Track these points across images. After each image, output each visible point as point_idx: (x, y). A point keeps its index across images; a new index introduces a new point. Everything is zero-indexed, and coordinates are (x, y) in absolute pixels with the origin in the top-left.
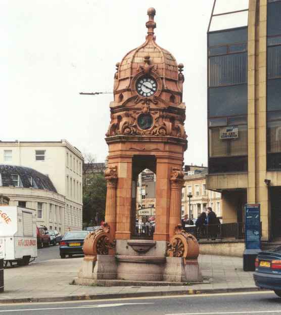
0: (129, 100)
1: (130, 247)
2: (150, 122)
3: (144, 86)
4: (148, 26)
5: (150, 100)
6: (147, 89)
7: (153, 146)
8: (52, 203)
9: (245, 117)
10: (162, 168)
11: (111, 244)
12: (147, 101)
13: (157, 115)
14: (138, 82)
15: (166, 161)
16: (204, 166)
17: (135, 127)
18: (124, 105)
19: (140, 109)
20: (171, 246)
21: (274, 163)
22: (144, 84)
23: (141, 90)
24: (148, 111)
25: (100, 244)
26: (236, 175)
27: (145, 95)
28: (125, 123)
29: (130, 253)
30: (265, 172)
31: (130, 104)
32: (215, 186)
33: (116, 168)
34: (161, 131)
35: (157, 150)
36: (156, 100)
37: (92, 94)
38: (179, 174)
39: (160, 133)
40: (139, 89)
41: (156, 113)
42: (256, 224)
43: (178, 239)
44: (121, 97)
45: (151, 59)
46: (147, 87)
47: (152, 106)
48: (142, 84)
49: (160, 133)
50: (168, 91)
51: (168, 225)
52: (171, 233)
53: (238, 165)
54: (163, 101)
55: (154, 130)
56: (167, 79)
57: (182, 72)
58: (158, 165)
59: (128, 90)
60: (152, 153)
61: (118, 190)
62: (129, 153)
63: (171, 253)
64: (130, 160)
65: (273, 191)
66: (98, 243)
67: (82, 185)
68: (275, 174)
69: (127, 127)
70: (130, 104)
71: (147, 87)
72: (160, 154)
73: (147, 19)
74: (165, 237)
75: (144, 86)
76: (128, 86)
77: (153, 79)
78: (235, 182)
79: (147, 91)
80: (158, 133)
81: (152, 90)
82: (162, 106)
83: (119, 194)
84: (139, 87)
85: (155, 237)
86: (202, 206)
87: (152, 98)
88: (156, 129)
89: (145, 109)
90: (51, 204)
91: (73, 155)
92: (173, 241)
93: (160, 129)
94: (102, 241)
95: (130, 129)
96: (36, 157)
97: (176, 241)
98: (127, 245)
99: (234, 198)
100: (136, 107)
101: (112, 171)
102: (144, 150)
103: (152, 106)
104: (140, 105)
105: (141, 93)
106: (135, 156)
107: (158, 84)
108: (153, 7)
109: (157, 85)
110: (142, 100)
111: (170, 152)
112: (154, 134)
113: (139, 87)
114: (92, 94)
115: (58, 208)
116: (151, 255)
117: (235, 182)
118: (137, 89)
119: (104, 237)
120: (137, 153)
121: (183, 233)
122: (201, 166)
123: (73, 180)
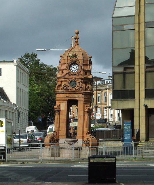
0: (66, 74)
2: (76, 84)
3: (73, 67)
5: (76, 74)
6: (74, 69)
7: (77, 95)
8: (7, 110)
10: (81, 105)
13: (78, 81)
14: (70, 66)
18: (64, 76)
19: (71, 78)
20: (84, 142)
21: (150, 94)
23: (72, 69)
26: (126, 101)
27: (73, 71)
28: (64, 85)
29: (67, 145)
30: (144, 99)
31: (67, 76)
32: (116, 106)
33: (60, 105)
34: (80, 89)
36: (78, 74)
38: (88, 109)
41: (79, 80)
43: (87, 138)
46: (74, 68)
47: (77, 77)
48: (72, 67)
51: (83, 132)
52: (85, 135)
53: (130, 95)
55: (77, 88)
57: (91, 60)
59: (65, 69)
60: (76, 99)
61: (61, 116)
62: (66, 98)
63: (84, 145)
65: (150, 112)
66: (51, 140)
67: (28, 94)
70: (67, 76)
71: (74, 68)
74: (82, 137)
75: (73, 67)
76: (66, 67)
78: (128, 105)
80: (79, 90)
82: (81, 77)
83: (61, 118)
85: (77, 137)
87: (76, 74)
89: (73, 79)
90: (6, 111)
91: (22, 71)
92: (85, 139)
93: (80, 88)
97: (87, 139)
99: (128, 114)
100: (69, 77)
101: (58, 106)
102: (73, 97)
103: (77, 77)
104: (71, 76)
105: (72, 70)
109: (79, 67)
110: (72, 74)
115: (11, 113)
117: (128, 105)
118: (70, 69)
119: (54, 137)
123: (19, 89)
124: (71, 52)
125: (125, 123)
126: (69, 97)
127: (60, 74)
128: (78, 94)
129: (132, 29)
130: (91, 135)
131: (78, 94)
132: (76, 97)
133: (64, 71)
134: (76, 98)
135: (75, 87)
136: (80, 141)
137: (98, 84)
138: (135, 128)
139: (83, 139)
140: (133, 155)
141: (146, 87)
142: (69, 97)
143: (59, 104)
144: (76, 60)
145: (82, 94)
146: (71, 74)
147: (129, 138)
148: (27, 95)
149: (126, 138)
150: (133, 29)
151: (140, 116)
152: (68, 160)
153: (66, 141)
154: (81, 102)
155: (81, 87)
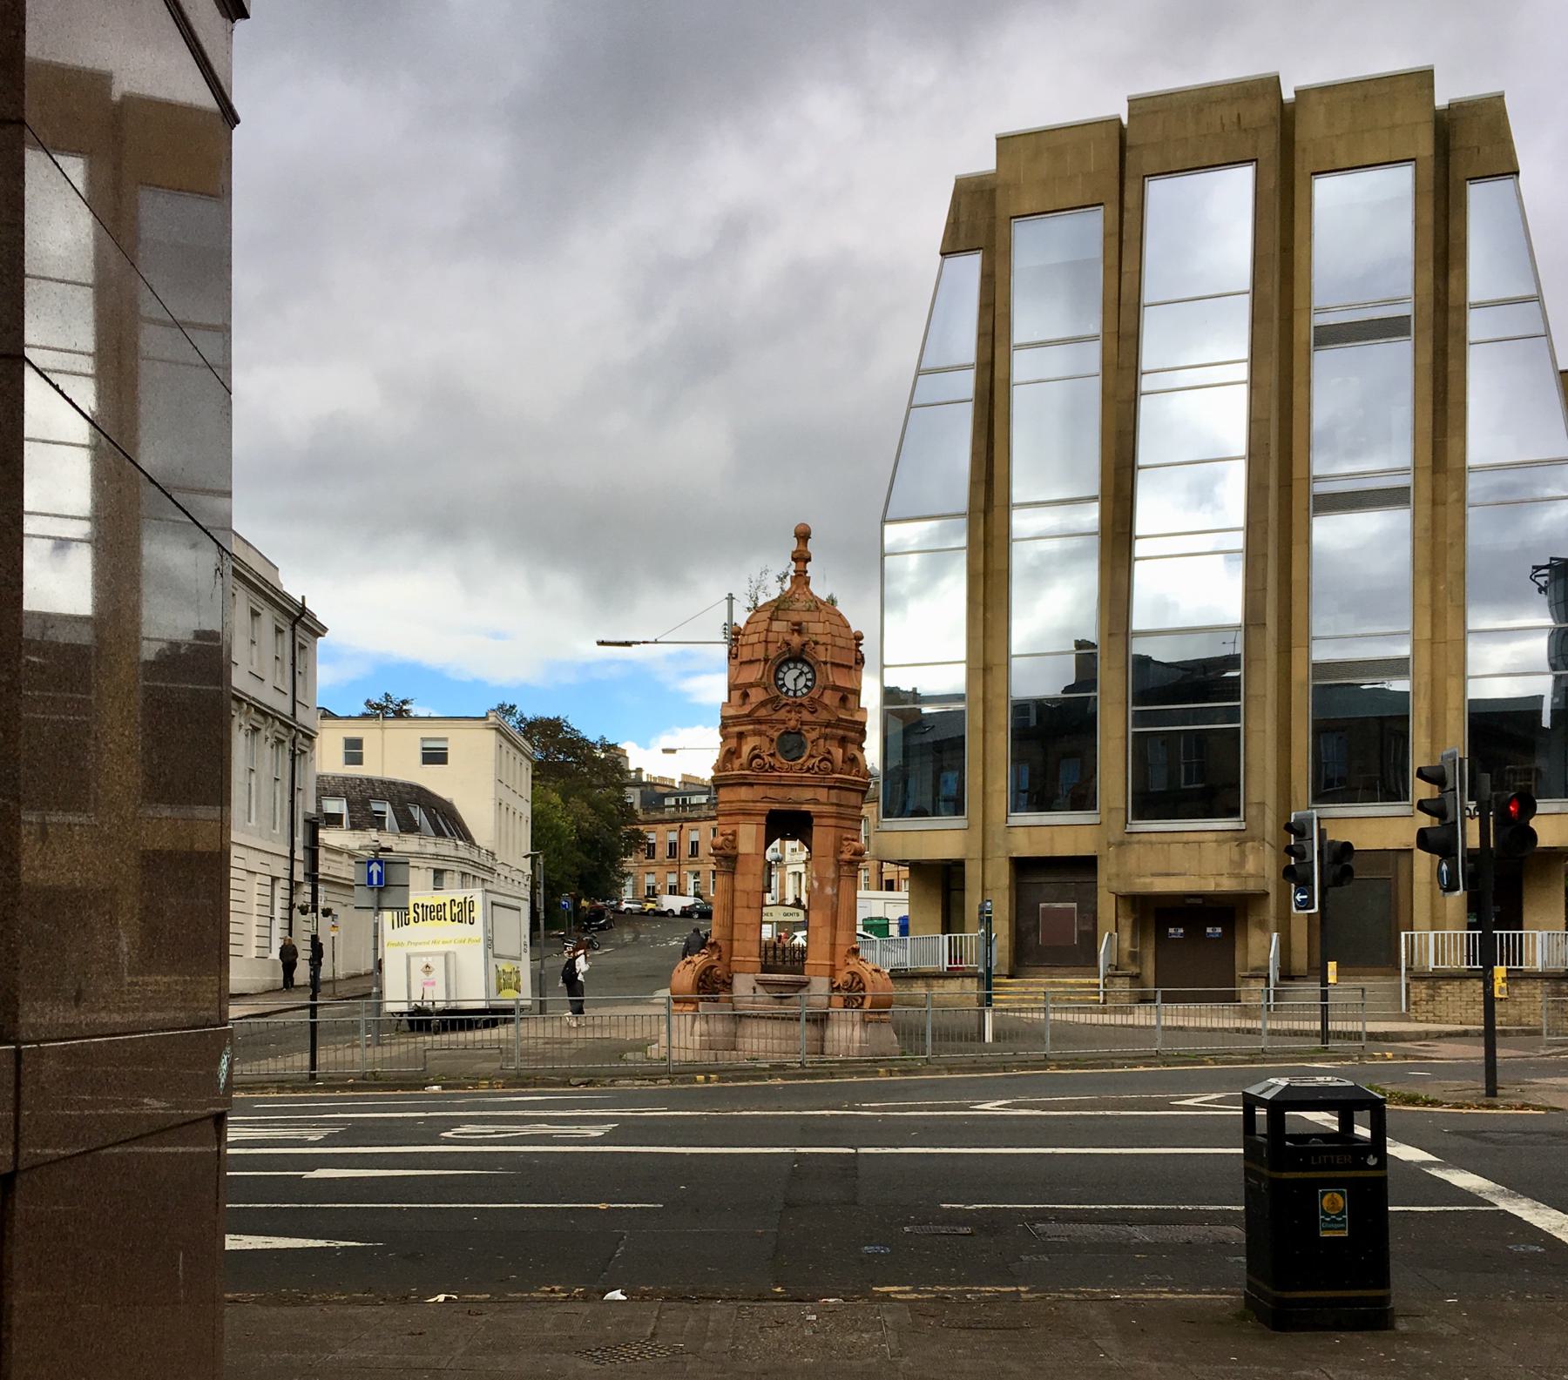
0: (763, 704)
5: (801, 705)
7: (808, 794)
15: (831, 822)
17: (772, 755)
28: (754, 749)
31: (762, 712)
34: (823, 765)
35: (816, 802)
36: (814, 706)
44: (745, 696)
47: (806, 716)
56: (833, 664)
60: (805, 808)
64: (763, 820)
73: (793, 544)
82: (824, 716)
104: (782, 714)
106: (771, 811)
120: (776, 806)
132: (805, 798)
139: (832, 975)
143: (734, 827)
145: (830, 788)
148: (808, 802)
153: (763, 983)
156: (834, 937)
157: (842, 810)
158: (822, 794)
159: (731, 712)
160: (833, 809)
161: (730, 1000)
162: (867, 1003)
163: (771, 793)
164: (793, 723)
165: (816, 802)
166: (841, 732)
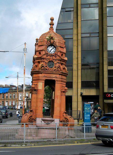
0: (44, 55)
1: (43, 122)
3: (52, 49)
4: (50, 25)
5: (53, 55)
7: (54, 76)
9: (82, 65)
11: (34, 120)
12: (52, 55)
15: (60, 82)
16: (30, 85)
22: (53, 49)
24: (52, 60)
25: (30, 120)
28: (42, 65)
31: (45, 57)
34: (58, 69)
35: (56, 77)
36: (55, 55)
37: (4, 52)
39: (58, 70)
40: (48, 50)
42: (88, 112)
45: (53, 38)
46: (51, 50)
47: (54, 58)
49: (58, 70)
50: (61, 52)
51: (60, 111)
54: (59, 56)
58: (56, 84)
60: (54, 79)
64: (44, 81)
68: (85, 90)
69: (43, 67)
71: (51, 50)
72: (58, 79)
73: (50, 21)
74: (59, 117)
75: (52, 49)
77: (54, 46)
79: (53, 50)
81: (50, 51)
82: (58, 58)
84: (48, 49)
86: (29, 102)
88: (56, 68)
93: (57, 68)
94: (31, 118)
95: (44, 67)
96: (108, 77)
98: (41, 120)
104: (49, 57)
106: (46, 80)
107: (57, 49)
108: (53, 17)
110: (50, 55)
111: (61, 78)
112: (55, 70)
113: (48, 49)
114: (4, 52)
116: (52, 125)
119: (31, 116)
120: (47, 78)
121: (67, 115)
122: (29, 85)
124: (48, 35)
125: (85, 105)
126: (46, 77)
127: (36, 56)
128: (55, 74)
129: (71, 38)
130: (68, 115)
131: (55, 74)
132: (53, 77)
133: (41, 52)
134: (53, 78)
135: (52, 67)
136: (57, 121)
137: (14, 89)
138: (72, 110)
140: (83, 132)
141: (81, 80)
142: (46, 77)
144: (54, 42)
145: (60, 74)
146: (49, 54)
147: (89, 118)
149: (86, 118)
150: (72, 38)
151: (76, 103)
152: (49, 141)
153: (44, 120)
154: (58, 82)
155: (58, 68)
156: (61, 109)
157: (62, 80)
158: (58, 76)
159: (36, 57)
160: (60, 79)
161: (36, 124)
162: (69, 125)
163: (46, 75)
164: (51, 59)
165: (56, 77)
166: (62, 62)
